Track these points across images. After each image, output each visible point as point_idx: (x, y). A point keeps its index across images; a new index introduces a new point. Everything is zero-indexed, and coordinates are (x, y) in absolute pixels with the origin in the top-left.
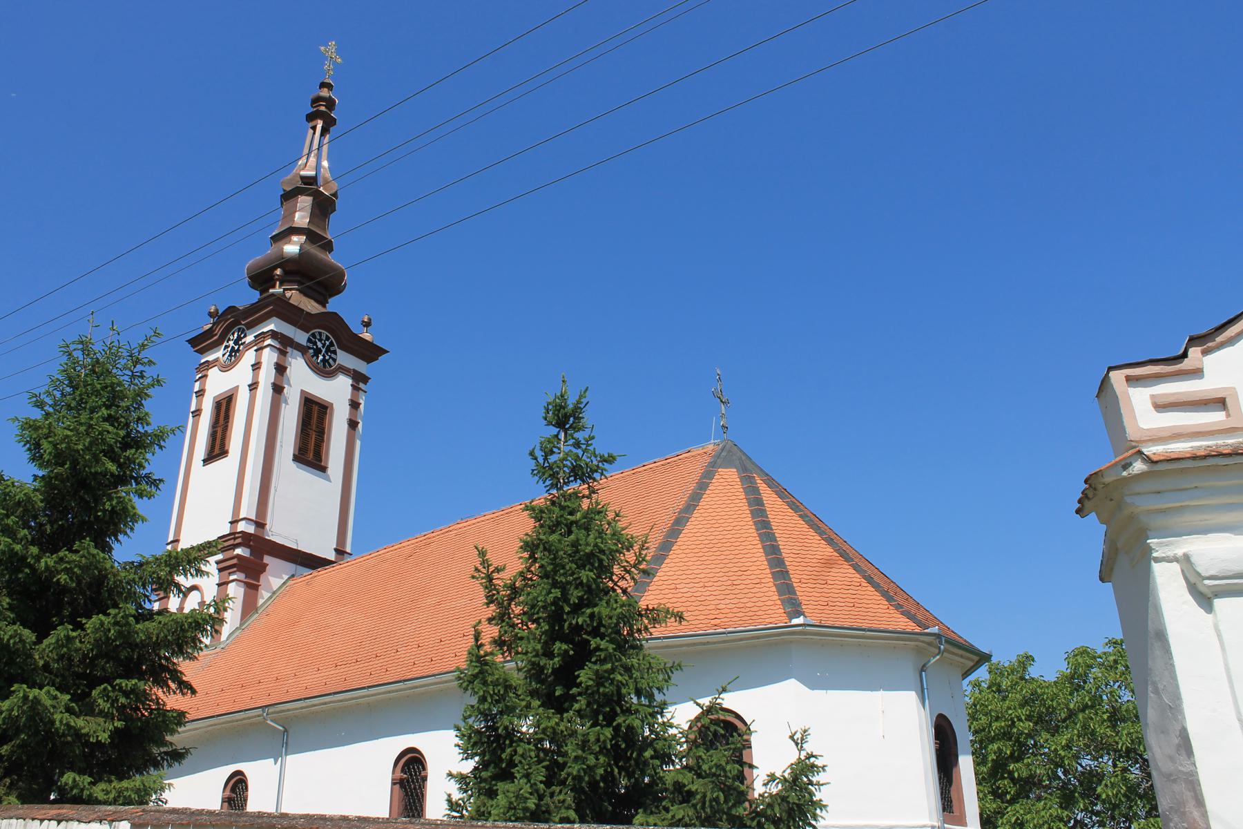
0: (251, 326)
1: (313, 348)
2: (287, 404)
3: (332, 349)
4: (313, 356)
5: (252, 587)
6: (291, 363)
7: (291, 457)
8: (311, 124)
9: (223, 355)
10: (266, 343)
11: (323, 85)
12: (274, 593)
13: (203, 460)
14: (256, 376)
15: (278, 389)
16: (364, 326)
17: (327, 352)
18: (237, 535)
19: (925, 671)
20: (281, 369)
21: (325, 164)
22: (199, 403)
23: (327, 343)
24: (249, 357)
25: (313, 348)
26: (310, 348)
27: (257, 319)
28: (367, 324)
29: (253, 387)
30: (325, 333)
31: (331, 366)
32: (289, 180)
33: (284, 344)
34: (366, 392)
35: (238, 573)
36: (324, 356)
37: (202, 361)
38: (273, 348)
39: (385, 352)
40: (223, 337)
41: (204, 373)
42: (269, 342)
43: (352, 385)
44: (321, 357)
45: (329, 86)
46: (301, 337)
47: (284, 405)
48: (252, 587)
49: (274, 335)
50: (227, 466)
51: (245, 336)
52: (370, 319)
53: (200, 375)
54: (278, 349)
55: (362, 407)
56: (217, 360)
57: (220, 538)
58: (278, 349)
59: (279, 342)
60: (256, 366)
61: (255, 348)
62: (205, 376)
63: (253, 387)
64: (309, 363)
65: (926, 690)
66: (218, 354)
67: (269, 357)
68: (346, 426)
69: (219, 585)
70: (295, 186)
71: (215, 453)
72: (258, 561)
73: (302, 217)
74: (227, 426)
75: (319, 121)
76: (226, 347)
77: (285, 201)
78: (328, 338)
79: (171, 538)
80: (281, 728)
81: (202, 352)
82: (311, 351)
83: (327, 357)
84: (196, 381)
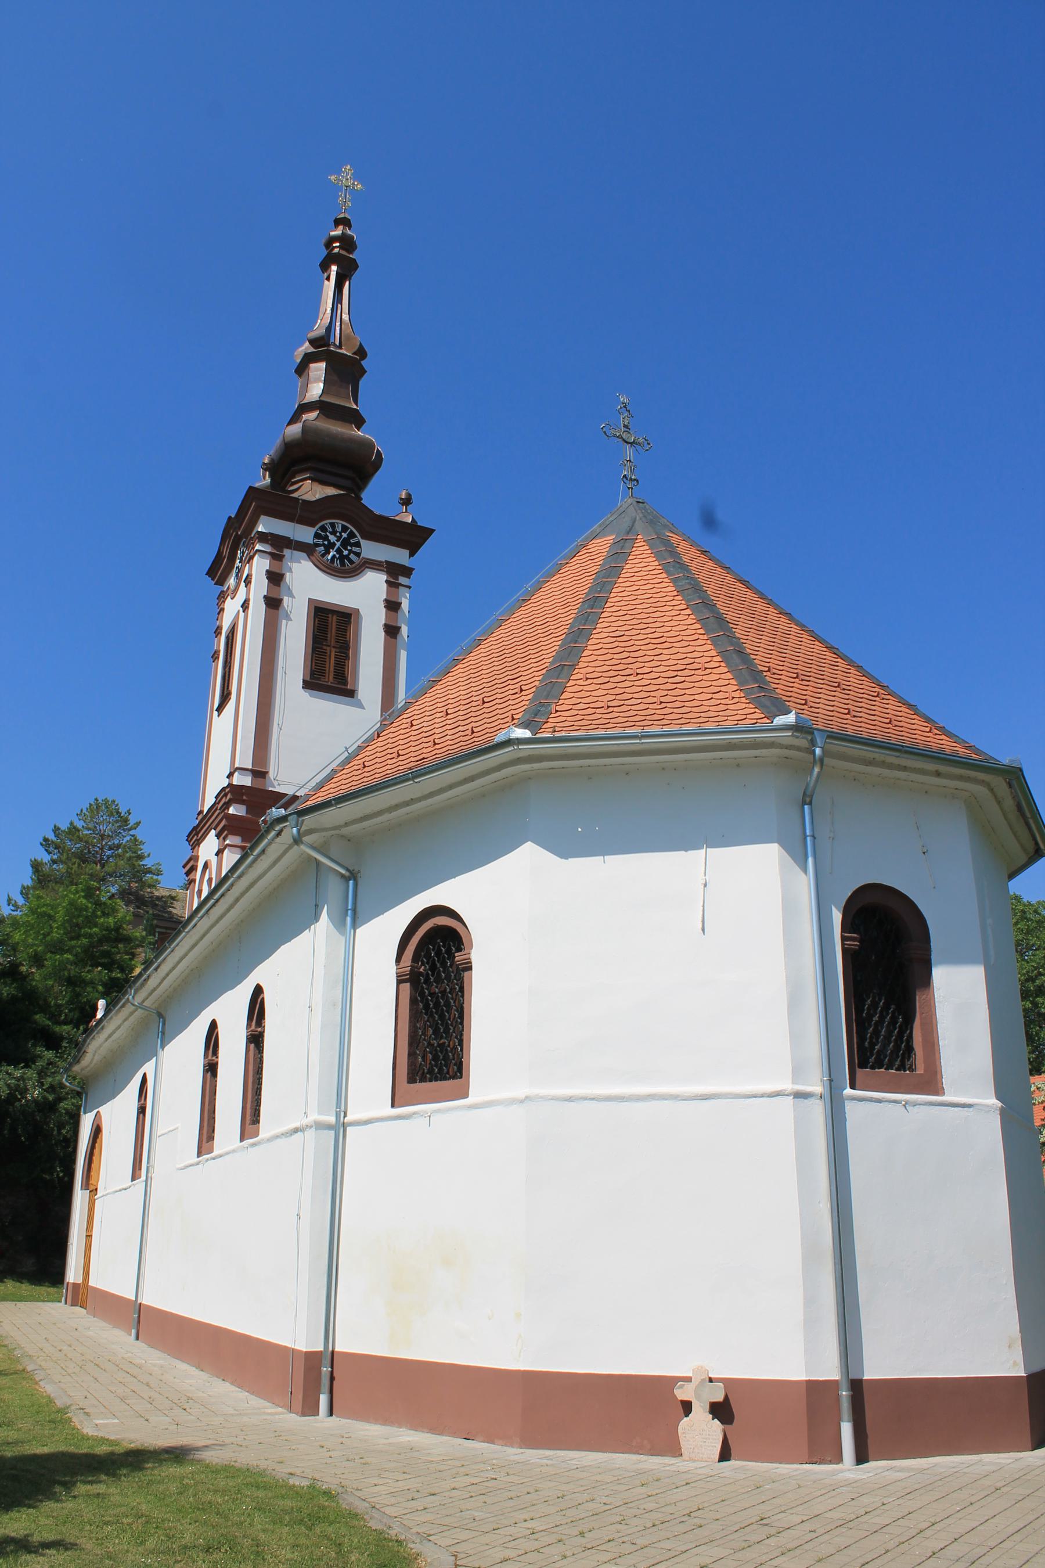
8: (326, 275)
15: (273, 603)
19: (810, 803)
20: (275, 578)
23: (345, 535)
25: (323, 545)
28: (407, 502)
30: (339, 523)
31: (351, 562)
33: (279, 545)
35: (230, 836)
39: (433, 531)
43: (387, 581)
45: (345, 222)
46: (305, 534)
47: (284, 622)
57: (216, 797)
59: (272, 545)
65: (809, 839)
69: (217, 854)
78: (344, 529)
82: (322, 548)
83: (345, 553)
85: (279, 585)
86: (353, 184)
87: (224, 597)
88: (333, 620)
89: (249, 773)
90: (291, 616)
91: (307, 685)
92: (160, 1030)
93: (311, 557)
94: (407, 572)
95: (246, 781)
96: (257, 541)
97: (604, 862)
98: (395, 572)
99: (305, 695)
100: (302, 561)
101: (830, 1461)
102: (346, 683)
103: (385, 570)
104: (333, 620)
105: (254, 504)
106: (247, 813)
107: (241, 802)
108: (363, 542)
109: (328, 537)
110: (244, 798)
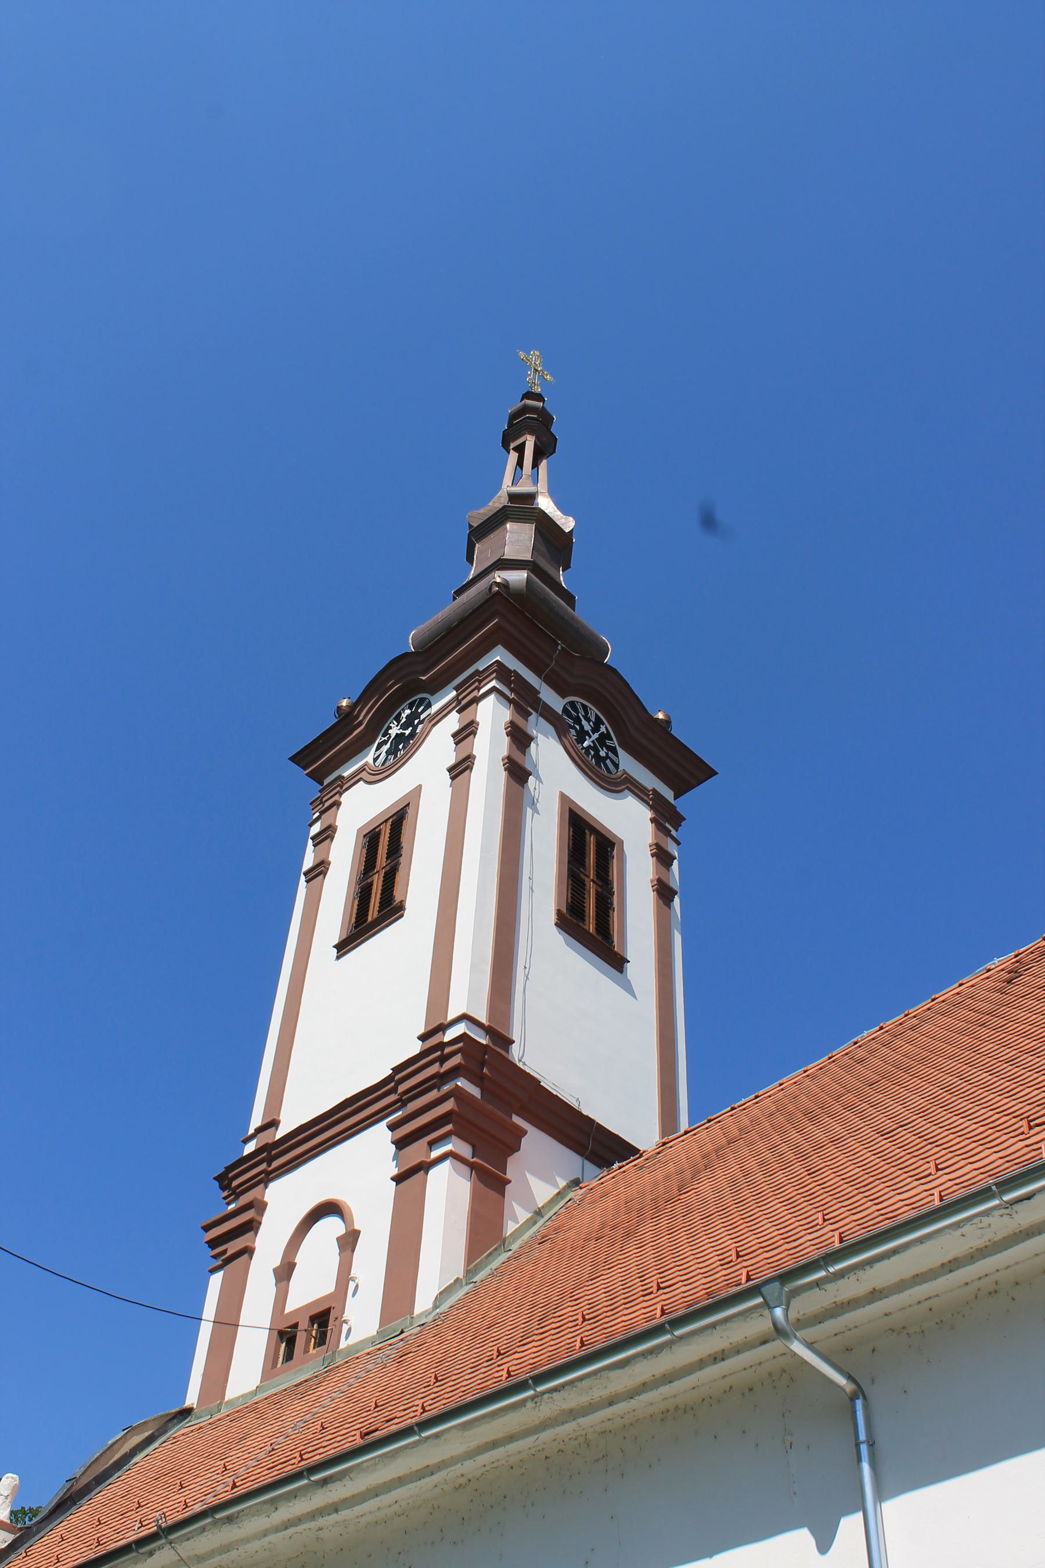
1: (574, 728)
2: (536, 811)
7: (553, 918)
9: (375, 760)
11: (528, 395)
12: (539, 1213)
13: (335, 947)
18: (447, 1050)
30: (594, 711)
35: (454, 1138)
40: (377, 725)
43: (652, 820)
47: (529, 811)
57: (397, 1070)
60: (465, 733)
61: (281, 1133)
62: (337, 804)
69: (398, 1179)
70: (503, 505)
72: (505, 1117)
77: (478, 540)
78: (598, 722)
80: (841, 1380)
90: (538, 806)
92: (862, 1437)
93: (564, 740)
96: (494, 675)
103: (651, 802)
105: (497, 620)
107: (477, 1079)
108: (620, 751)
109: (581, 721)
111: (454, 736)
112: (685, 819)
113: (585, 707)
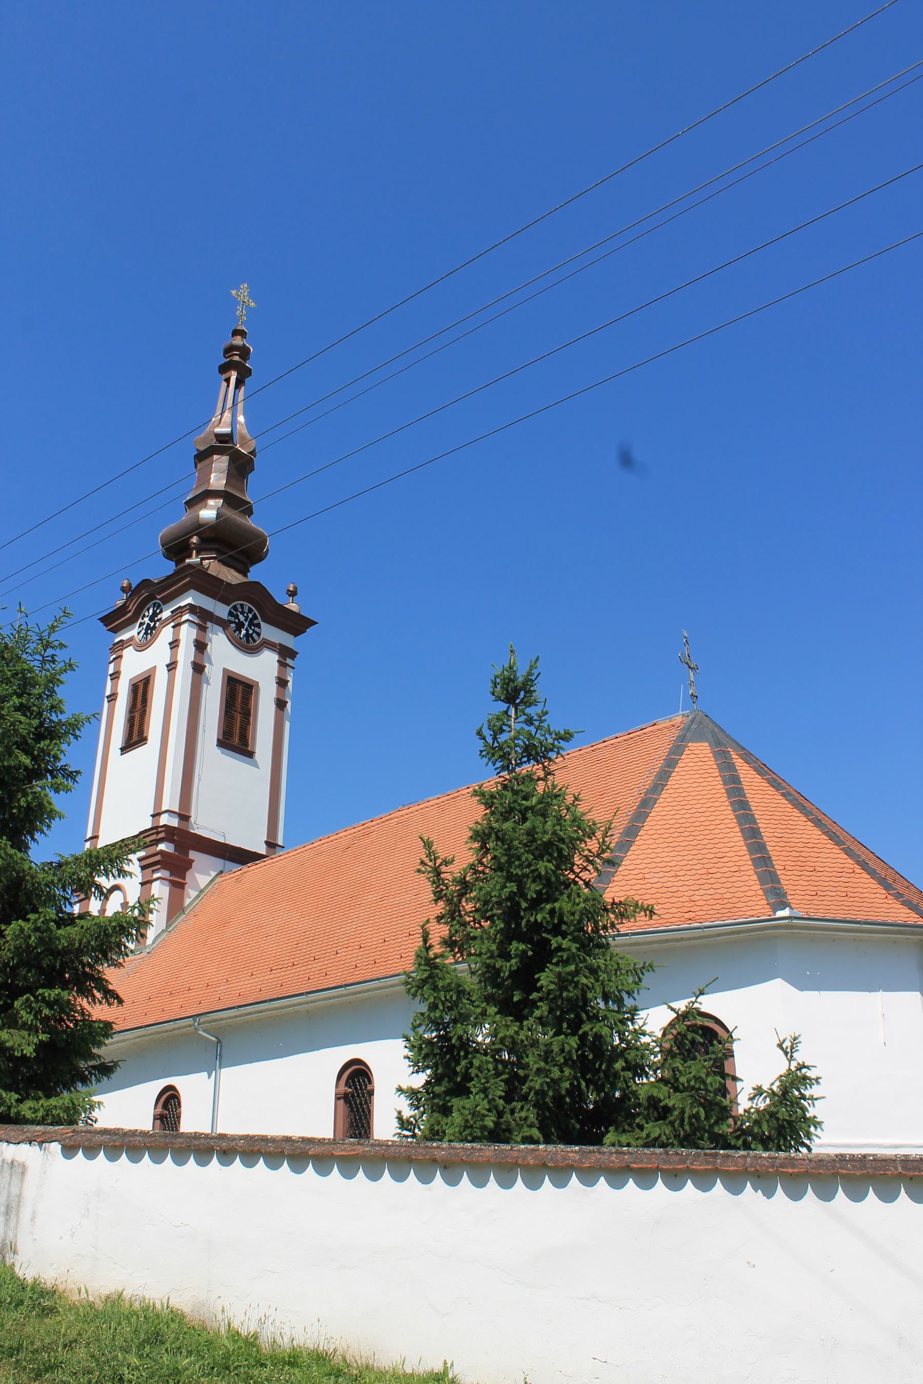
0: (167, 600)
1: (234, 622)
2: (208, 684)
3: (255, 622)
4: (235, 631)
5: (178, 886)
6: (211, 639)
8: (224, 376)
9: (139, 633)
10: (184, 618)
11: (236, 333)
12: (201, 891)
14: (174, 655)
15: (198, 668)
16: (290, 596)
17: (250, 625)
18: (159, 830)
20: (200, 646)
21: (241, 419)
22: (114, 687)
23: (250, 616)
24: (166, 634)
25: (234, 622)
26: (232, 622)
27: (175, 590)
28: (293, 594)
29: (172, 666)
30: (247, 605)
31: (255, 641)
32: (203, 439)
33: (204, 618)
34: (294, 668)
35: (162, 870)
36: (247, 630)
37: (117, 640)
38: (190, 623)
41: (119, 653)
42: (187, 617)
43: (278, 661)
44: (244, 632)
45: (242, 334)
46: (222, 610)
47: (205, 685)
48: (178, 886)
49: (192, 609)
50: (147, 753)
51: (161, 612)
52: (296, 588)
53: (114, 656)
54: (198, 624)
55: (290, 685)
56: (132, 639)
57: (141, 833)
58: (198, 624)
59: (198, 617)
60: (174, 644)
62: (120, 657)
63: (172, 666)
64: (231, 638)
66: (133, 632)
67: (188, 634)
68: (274, 706)
69: (142, 884)
71: (133, 741)
73: (219, 479)
74: (145, 711)
75: (233, 372)
76: (142, 624)
77: (199, 462)
78: (250, 611)
79: (89, 835)
81: (115, 630)
82: (233, 625)
83: (251, 632)
84: (110, 663)
85: (203, 653)
86: (248, 301)
87: (122, 646)
88: (240, 688)
89: (176, 816)
91: (221, 744)
94: (292, 654)
95: (174, 822)
97: (736, 1027)
98: (286, 653)
99: (218, 751)
100: (219, 634)
101: (156, 1338)
102: (247, 745)
104: (240, 688)
106: (175, 851)
108: (263, 624)
110: (175, 838)
111: (170, 644)
112: (194, 861)
113: (242, 606)
